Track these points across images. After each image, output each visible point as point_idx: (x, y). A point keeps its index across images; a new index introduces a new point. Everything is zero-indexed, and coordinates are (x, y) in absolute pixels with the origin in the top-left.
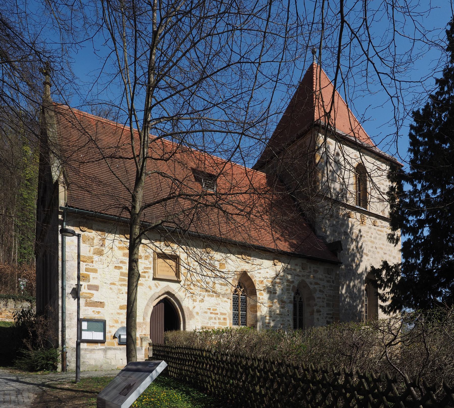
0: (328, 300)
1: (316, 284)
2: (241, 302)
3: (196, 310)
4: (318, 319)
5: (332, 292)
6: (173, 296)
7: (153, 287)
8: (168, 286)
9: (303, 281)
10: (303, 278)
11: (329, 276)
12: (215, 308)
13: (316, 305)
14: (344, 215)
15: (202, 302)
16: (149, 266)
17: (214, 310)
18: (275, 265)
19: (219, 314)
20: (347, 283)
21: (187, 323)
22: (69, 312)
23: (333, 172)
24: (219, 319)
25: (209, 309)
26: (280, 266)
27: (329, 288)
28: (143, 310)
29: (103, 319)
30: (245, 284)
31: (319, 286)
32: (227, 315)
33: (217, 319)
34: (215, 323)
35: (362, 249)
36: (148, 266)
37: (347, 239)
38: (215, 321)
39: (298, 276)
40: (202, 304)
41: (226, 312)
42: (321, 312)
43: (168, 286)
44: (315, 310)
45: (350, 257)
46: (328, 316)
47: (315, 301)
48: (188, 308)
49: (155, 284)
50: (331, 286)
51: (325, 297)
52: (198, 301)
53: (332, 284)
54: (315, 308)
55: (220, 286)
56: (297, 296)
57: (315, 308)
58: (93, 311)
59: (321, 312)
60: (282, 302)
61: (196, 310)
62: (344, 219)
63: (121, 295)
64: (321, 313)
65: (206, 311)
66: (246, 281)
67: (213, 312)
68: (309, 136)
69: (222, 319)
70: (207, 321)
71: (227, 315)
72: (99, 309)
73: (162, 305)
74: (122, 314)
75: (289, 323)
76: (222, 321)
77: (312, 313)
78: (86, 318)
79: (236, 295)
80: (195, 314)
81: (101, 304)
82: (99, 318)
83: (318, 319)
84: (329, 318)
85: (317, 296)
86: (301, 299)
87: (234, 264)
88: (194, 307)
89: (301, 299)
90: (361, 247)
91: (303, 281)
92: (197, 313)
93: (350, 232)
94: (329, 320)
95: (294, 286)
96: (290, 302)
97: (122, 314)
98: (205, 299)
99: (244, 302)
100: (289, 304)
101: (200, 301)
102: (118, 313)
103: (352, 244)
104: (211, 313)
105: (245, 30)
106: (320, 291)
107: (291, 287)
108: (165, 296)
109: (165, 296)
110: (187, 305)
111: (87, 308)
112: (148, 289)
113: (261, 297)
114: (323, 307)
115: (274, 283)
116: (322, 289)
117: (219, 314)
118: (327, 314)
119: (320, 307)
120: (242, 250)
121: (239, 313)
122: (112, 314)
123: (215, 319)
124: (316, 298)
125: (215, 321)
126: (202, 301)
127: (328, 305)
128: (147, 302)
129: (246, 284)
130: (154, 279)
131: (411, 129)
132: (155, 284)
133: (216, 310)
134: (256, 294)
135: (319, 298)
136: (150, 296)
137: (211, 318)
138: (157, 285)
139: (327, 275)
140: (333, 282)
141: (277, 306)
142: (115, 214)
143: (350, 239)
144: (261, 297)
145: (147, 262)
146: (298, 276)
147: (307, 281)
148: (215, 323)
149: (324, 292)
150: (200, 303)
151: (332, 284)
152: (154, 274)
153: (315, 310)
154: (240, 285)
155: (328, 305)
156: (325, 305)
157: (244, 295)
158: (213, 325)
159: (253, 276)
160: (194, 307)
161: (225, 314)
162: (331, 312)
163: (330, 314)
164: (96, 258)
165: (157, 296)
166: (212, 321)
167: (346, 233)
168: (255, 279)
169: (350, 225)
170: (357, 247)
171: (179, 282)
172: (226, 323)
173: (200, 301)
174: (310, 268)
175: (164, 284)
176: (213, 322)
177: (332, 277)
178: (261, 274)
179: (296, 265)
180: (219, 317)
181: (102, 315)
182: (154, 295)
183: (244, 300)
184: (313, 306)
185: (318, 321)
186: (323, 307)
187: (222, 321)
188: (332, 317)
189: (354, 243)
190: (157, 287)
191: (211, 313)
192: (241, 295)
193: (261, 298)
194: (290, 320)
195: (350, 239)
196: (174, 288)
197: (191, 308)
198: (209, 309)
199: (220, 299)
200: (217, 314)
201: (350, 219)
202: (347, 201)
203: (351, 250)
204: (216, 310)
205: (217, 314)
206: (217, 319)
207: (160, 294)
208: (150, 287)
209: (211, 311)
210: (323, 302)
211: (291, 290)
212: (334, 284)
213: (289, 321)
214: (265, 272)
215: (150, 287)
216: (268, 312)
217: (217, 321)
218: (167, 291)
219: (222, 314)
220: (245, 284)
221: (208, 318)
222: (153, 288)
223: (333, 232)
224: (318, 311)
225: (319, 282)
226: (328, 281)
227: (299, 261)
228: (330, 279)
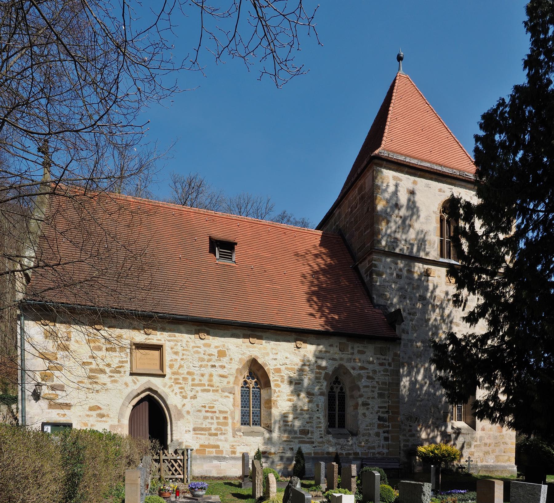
0: (379, 389)
1: (362, 368)
2: (253, 396)
3: (187, 408)
4: (364, 414)
5: (387, 378)
6: (156, 392)
7: (131, 384)
8: (149, 381)
9: (341, 366)
10: (342, 362)
11: (383, 357)
12: (212, 405)
13: (361, 396)
14: (421, 275)
15: (194, 399)
16: (125, 359)
17: (210, 407)
18: (298, 348)
19: (217, 412)
20: (427, 365)
21: (173, 425)
22: (29, 416)
23: (404, 219)
24: (218, 418)
25: (205, 407)
26: (309, 350)
27: (382, 373)
28: (118, 411)
29: (70, 422)
30: (257, 372)
31: (366, 371)
32: (229, 413)
33: (215, 418)
34: (212, 424)
35: (451, 319)
36: (123, 360)
37: (425, 305)
38: (212, 421)
39: (334, 359)
40: (194, 401)
41: (228, 410)
42: (369, 404)
43: (149, 381)
44: (360, 403)
45: (430, 329)
46: (381, 410)
47: (359, 391)
48: (176, 406)
49: (133, 380)
50: (386, 370)
51: (377, 385)
52: (189, 397)
53: (388, 367)
54: (360, 401)
55: (219, 379)
56: (337, 385)
57: (360, 401)
58: (58, 414)
59: (369, 404)
60: (309, 394)
61: (187, 408)
62: (421, 280)
63: (91, 394)
64: (370, 407)
65: (199, 409)
66: (258, 371)
67: (210, 410)
68: (369, 175)
69: (221, 418)
70: (200, 421)
71: (229, 413)
72: (66, 411)
73: (146, 404)
74: (92, 416)
75: (319, 420)
76: (221, 420)
77: (356, 407)
78: (50, 422)
79: (246, 388)
80: (184, 413)
81: (68, 406)
82: (65, 422)
83: (364, 414)
84: (383, 413)
85: (364, 384)
86: (342, 389)
87: (239, 350)
88: (184, 405)
89: (342, 389)
90: (449, 316)
91: (341, 366)
92: (188, 412)
93: (431, 296)
94: (382, 415)
95: (326, 374)
96: (322, 394)
97: (92, 416)
98: (198, 395)
99: (258, 397)
100: (319, 397)
101: (191, 398)
102: (88, 416)
103: (434, 311)
104: (207, 411)
105: (62, 43)
106: (368, 377)
107: (323, 375)
108: (147, 393)
109: (147, 393)
110: (174, 404)
111: (50, 410)
112: (124, 386)
113: (277, 390)
114: (373, 398)
115: (301, 371)
116: (371, 374)
117: (217, 412)
118: (380, 407)
119: (368, 398)
120: (249, 333)
121: (250, 410)
122: (80, 416)
123: (212, 418)
124: (361, 388)
125: (212, 421)
126: (194, 397)
127: (381, 395)
128: (123, 401)
129: (259, 374)
130: (131, 374)
131: (477, 141)
132: (133, 380)
133: (213, 407)
134: (270, 386)
135: (367, 387)
136: (126, 394)
137: (206, 418)
138: (136, 381)
139: (379, 356)
140: (390, 365)
141: (303, 401)
142: (78, 303)
143: (430, 306)
144: (277, 390)
145: (123, 354)
146: (334, 359)
147: (348, 365)
148: (212, 424)
149: (374, 379)
150: (192, 400)
151: (388, 367)
152: (131, 368)
153: (360, 403)
154: (251, 375)
155: (381, 395)
156: (376, 395)
157: (257, 388)
158: (210, 426)
159: (266, 364)
160: (184, 405)
161: (226, 412)
162: (386, 405)
163: (385, 407)
164: (60, 354)
165: (135, 394)
166: (208, 421)
167: (423, 298)
168: (269, 367)
169: (431, 287)
170: (442, 316)
171: (164, 376)
172: (227, 423)
173: (191, 398)
174: (353, 348)
175: (143, 381)
176: (209, 423)
177: (387, 358)
178: (277, 361)
179: (331, 346)
180: (217, 416)
181: (68, 418)
182: (131, 393)
183: (257, 394)
184: (357, 398)
185: (365, 416)
186: (373, 398)
187: (221, 420)
188: (387, 412)
189: (437, 310)
190: (135, 383)
191: (207, 411)
192: (253, 388)
193: (277, 391)
194: (321, 417)
195: (430, 306)
196: (157, 383)
197: (179, 407)
198: (205, 407)
199: (218, 395)
200: (215, 412)
201: (430, 278)
202: (427, 254)
203: (432, 321)
204: (213, 407)
205: (215, 412)
206: (215, 418)
207: (139, 392)
208: (126, 384)
209: (207, 409)
210: (373, 391)
211: (322, 378)
212: (392, 368)
213: (318, 418)
214: (284, 358)
215: (126, 384)
216: (291, 409)
217: (215, 421)
218: (147, 387)
219: (221, 412)
220: (257, 372)
221: (202, 417)
222: (130, 384)
223: (403, 298)
224: (365, 404)
225: (366, 365)
226: (381, 364)
227: (335, 340)
228: (384, 361)
